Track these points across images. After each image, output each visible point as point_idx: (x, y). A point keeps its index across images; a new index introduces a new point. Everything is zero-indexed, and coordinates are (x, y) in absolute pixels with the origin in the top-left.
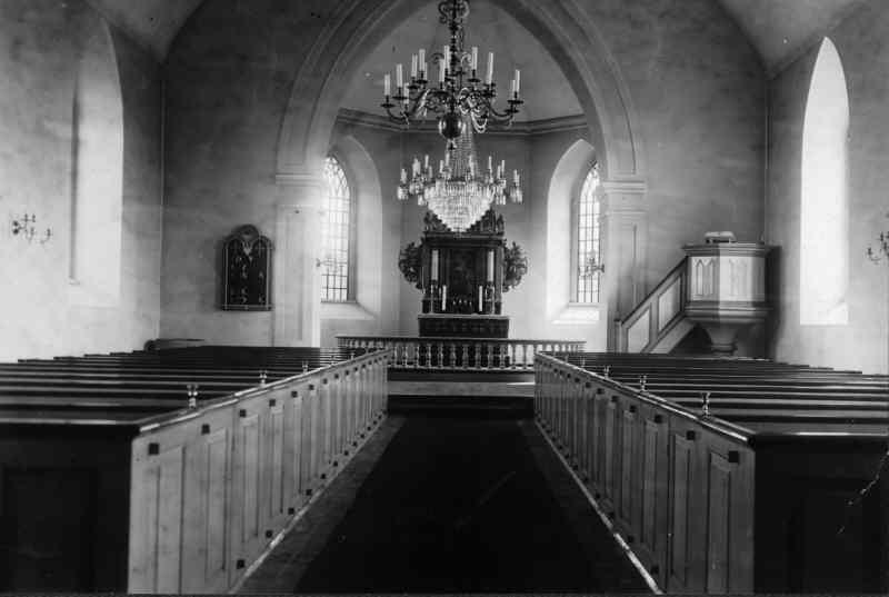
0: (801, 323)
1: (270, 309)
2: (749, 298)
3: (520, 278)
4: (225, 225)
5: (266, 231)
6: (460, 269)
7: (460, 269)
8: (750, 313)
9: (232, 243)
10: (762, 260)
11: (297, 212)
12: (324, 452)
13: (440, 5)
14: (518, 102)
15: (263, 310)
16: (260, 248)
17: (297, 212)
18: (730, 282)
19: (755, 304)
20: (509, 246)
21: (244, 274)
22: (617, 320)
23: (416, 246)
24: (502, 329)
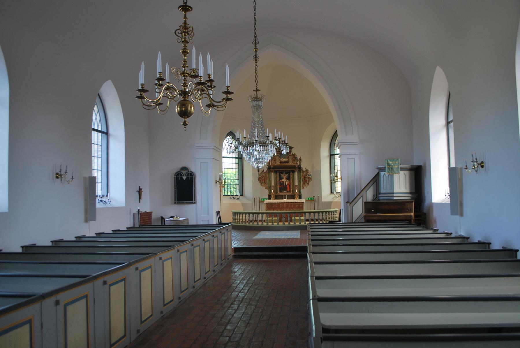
0: (433, 202)
1: (195, 203)
2: (408, 191)
3: (308, 184)
4: (176, 167)
5: (192, 169)
6: (283, 180)
7: (283, 180)
8: (409, 198)
9: (178, 175)
10: (413, 172)
11: (58, 176)
12: (311, 224)
13: (175, 33)
14: (146, 91)
15: (192, 203)
16: (189, 176)
17: (58, 176)
18: (400, 186)
19: (411, 193)
20: (304, 169)
21: (184, 189)
22: (347, 202)
23: (265, 171)
24: (301, 206)
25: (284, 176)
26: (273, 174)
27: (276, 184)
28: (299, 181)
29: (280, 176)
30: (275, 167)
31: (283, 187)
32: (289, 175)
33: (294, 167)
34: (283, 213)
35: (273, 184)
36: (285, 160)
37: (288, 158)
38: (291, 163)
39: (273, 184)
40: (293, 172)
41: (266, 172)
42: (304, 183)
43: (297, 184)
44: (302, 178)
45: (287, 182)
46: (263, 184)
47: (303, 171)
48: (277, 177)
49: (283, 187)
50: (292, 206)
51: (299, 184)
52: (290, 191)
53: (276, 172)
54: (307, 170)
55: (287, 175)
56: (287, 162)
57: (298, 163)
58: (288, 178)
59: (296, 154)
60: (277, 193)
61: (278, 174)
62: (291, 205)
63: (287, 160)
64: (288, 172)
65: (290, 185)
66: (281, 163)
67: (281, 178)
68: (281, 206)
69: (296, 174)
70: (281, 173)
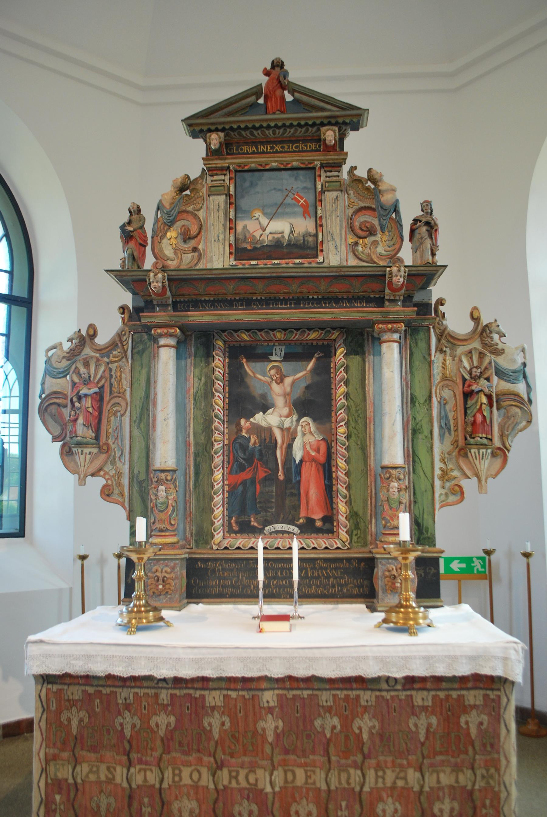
3: (502, 453)
6: (273, 419)
7: (273, 419)
20: (457, 322)
23: (102, 340)
24: (472, 722)
25: (279, 383)
26: (166, 358)
27: (199, 455)
28: (413, 432)
29: (236, 377)
30: (188, 288)
31: (264, 487)
32: (324, 370)
33: (370, 286)
34: (272, 328)
35: (166, 453)
36: (281, 227)
37: (311, 210)
38: (336, 255)
39: (166, 453)
40: (361, 340)
41: (116, 343)
42: (462, 451)
43: (393, 451)
44: (445, 398)
45: (306, 439)
46: (83, 457)
47: (448, 340)
48: (207, 393)
49: (264, 487)
50: (365, 725)
51: (412, 456)
52: (328, 525)
53: (197, 342)
54: (483, 331)
55: (302, 373)
56: (307, 247)
57: (407, 254)
58: (314, 404)
59: (389, 179)
60: (203, 536)
61: (219, 363)
62: (349, 711)
63: (304, 226)
64: (310, 348)
65: (327, 469)
66: (239, 252)
67: (244, 402)
68: (215, 723)
69: (391, 357)
70: (245, 350)
